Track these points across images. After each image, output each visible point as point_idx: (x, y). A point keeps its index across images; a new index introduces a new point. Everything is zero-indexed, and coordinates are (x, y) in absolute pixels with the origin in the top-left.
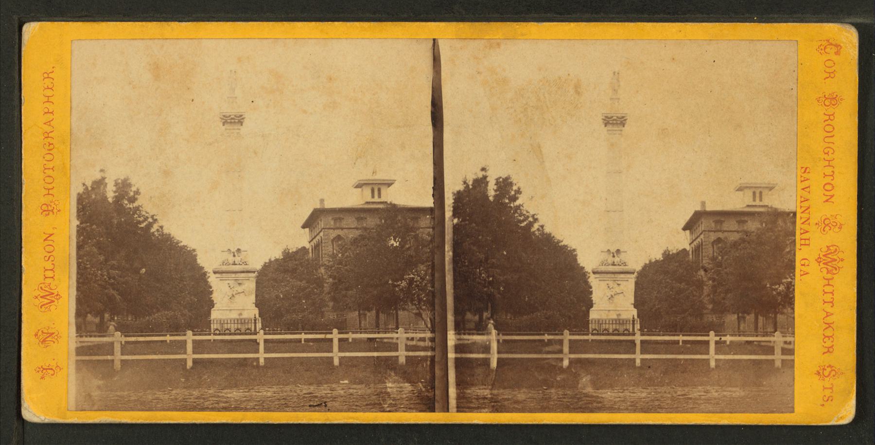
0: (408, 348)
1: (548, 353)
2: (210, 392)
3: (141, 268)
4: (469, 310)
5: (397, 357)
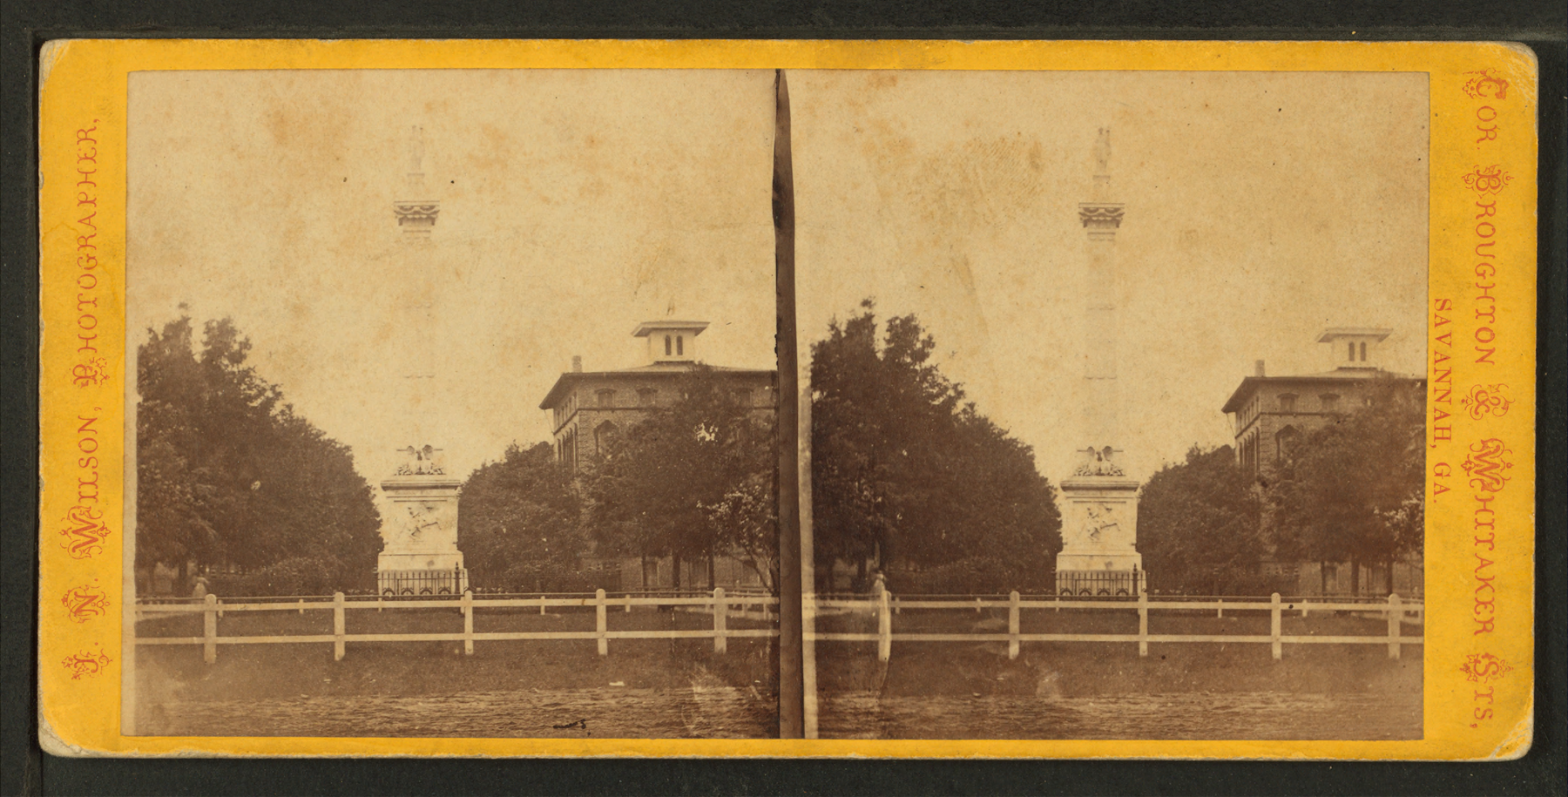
0: (732, 624)
1: (983, 631)
2: (377, 701)
3: (252, 481)
4: (162, 560)
5: (712, 639)
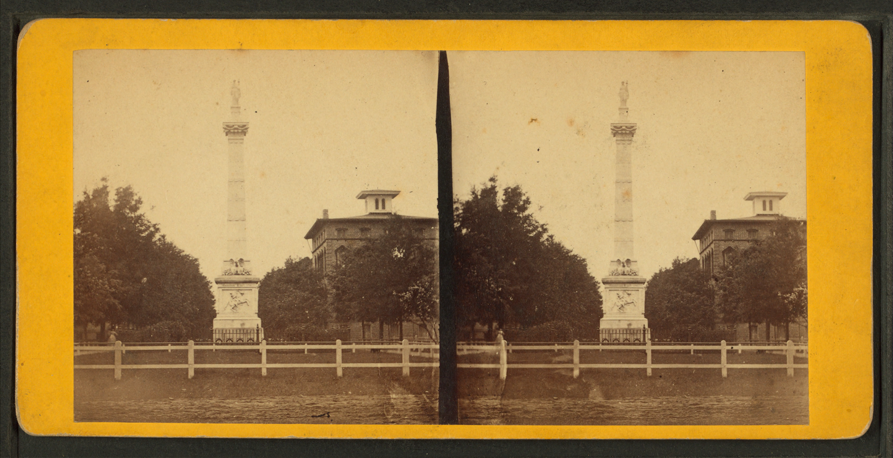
0: (412, 359)
1: (559, 363)
2: (212, 401)
3: (142, 278)
4: (91, 321)
5: (401, 368)
